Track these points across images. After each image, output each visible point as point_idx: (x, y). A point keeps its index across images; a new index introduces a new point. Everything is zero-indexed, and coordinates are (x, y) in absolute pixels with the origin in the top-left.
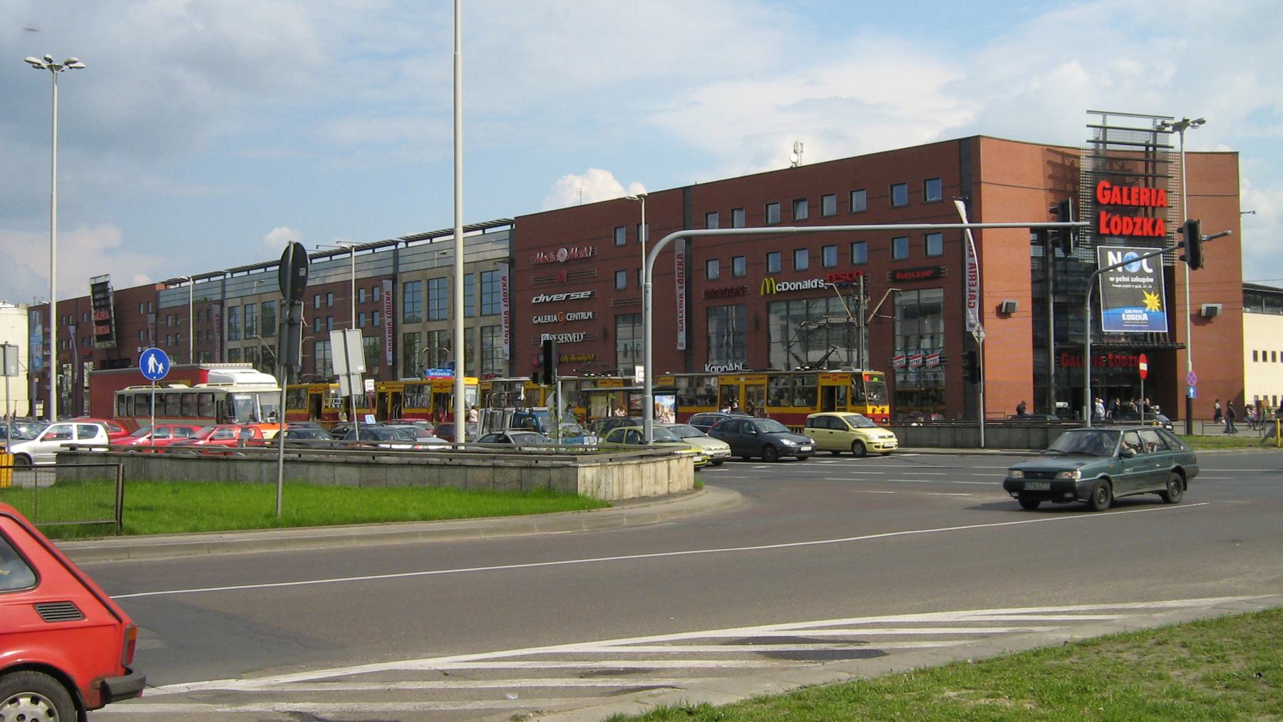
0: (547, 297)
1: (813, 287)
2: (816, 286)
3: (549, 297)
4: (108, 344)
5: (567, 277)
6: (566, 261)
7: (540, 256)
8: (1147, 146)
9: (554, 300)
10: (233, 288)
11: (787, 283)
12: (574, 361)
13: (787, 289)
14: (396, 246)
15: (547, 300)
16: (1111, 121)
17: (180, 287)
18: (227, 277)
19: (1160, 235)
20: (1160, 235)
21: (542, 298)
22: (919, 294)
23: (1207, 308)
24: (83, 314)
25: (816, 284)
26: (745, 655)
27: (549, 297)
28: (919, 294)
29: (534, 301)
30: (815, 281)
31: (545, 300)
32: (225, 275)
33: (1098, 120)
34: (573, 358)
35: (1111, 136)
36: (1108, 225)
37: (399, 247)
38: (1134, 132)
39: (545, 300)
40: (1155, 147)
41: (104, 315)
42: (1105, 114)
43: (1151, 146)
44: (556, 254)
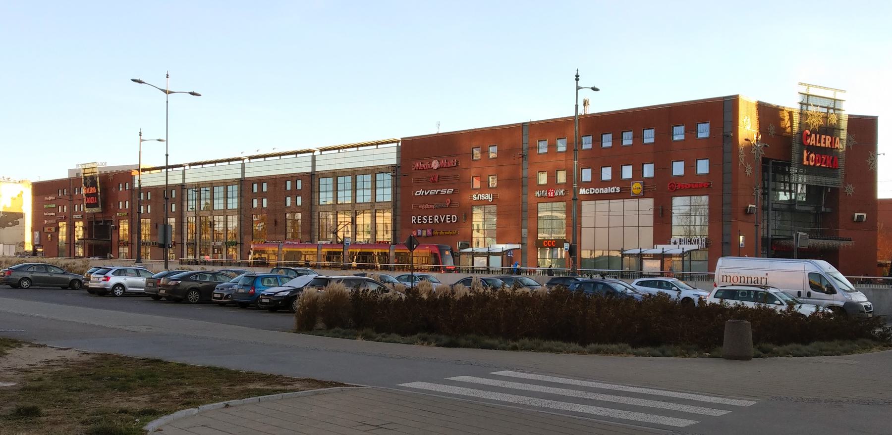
0: (425, 191)
1: (612, 192)
2: (614, 191)
3: (427, 192)
4: (95, 210)
5: (438, 179)
6: (438, 169)
7: (418, 165)
9: (430, 194)
10: (191, 176)
11: (593, 189)
12: (442, 235)
13: (593, 192)
14: (313, 154)
15: (426, 194)
16: (812, 91)
17: (173, 171)
18: (245, 162)
19: (837, 147)
20: (837, 147)
21: (421, 192)
22: (488, 264)
23: (858, 216)
24: (126, 184)
25: (614, 190)
26: (665, 285)
27: (427, 192)
28: (488, 264)
29: (416, 194)
30: (613, 188)
31: (424, 193)
32: (243, 160)
34: (442, 233)
36: (808, 159)
37: (315, 154)
38: (824, 99)
39: (424, 193)
41: (92, 190)
42: (808, 85)
43: (831, 108)
44: (430, 163)
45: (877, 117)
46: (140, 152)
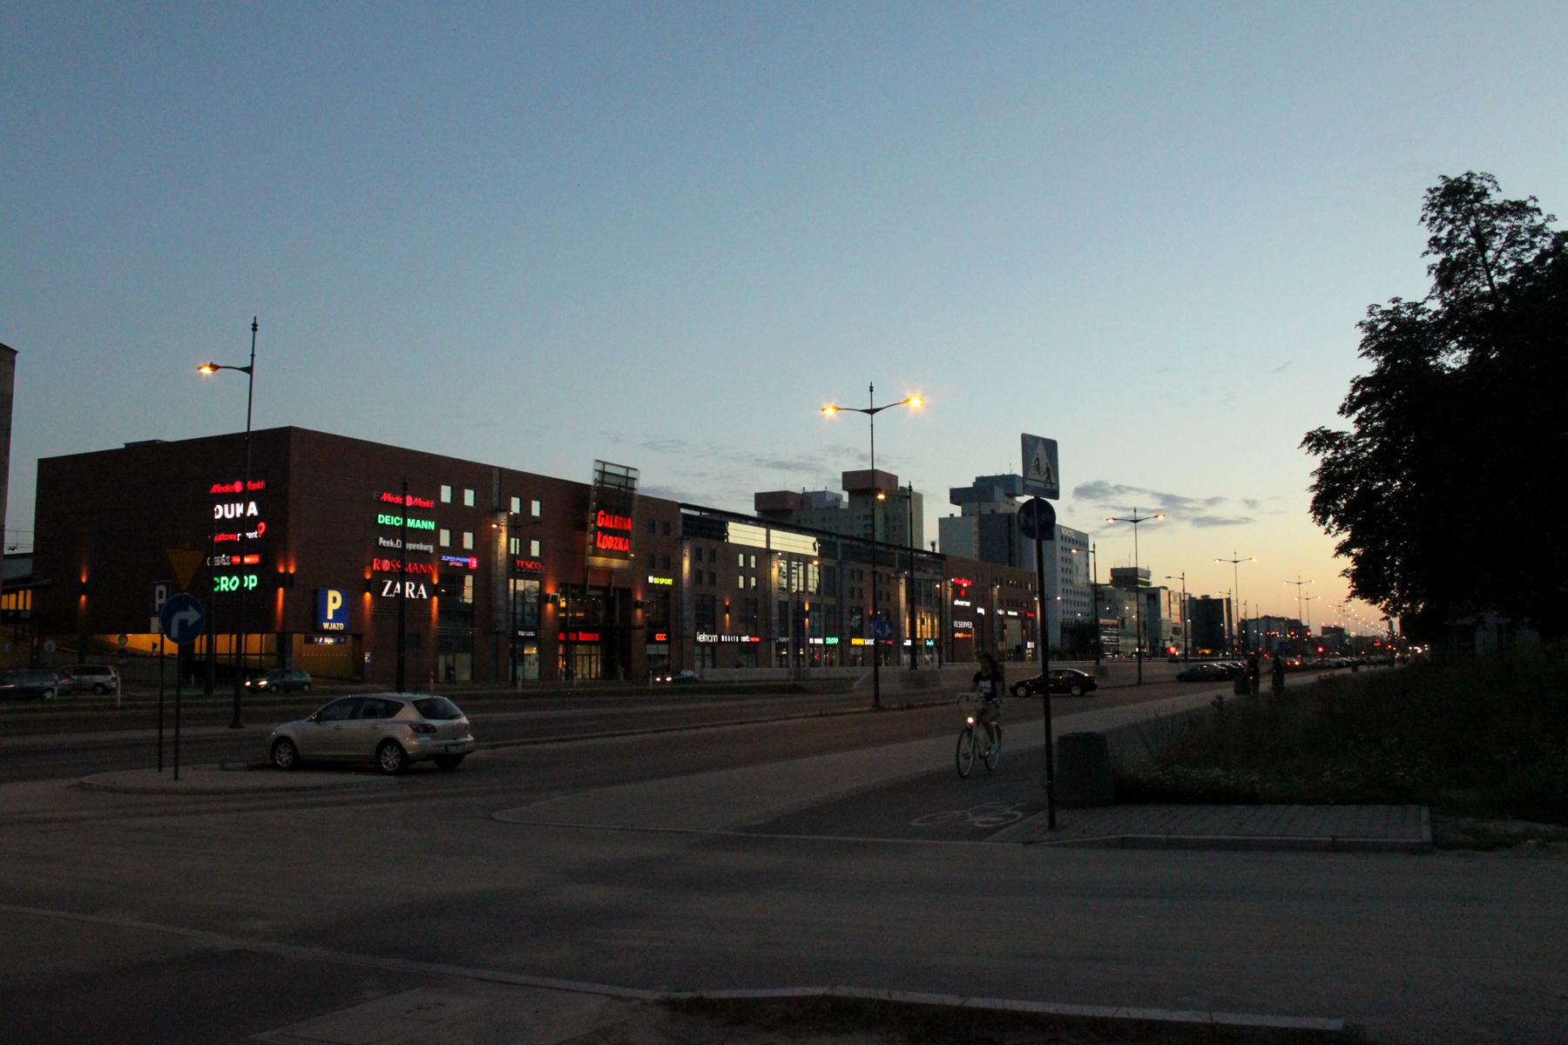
8: (620, 486)
16: (608, 469)
33: (600, 467)
35: (607, 479)
40: (626, 487)
45: (42, 462)
46: (872, 426)
